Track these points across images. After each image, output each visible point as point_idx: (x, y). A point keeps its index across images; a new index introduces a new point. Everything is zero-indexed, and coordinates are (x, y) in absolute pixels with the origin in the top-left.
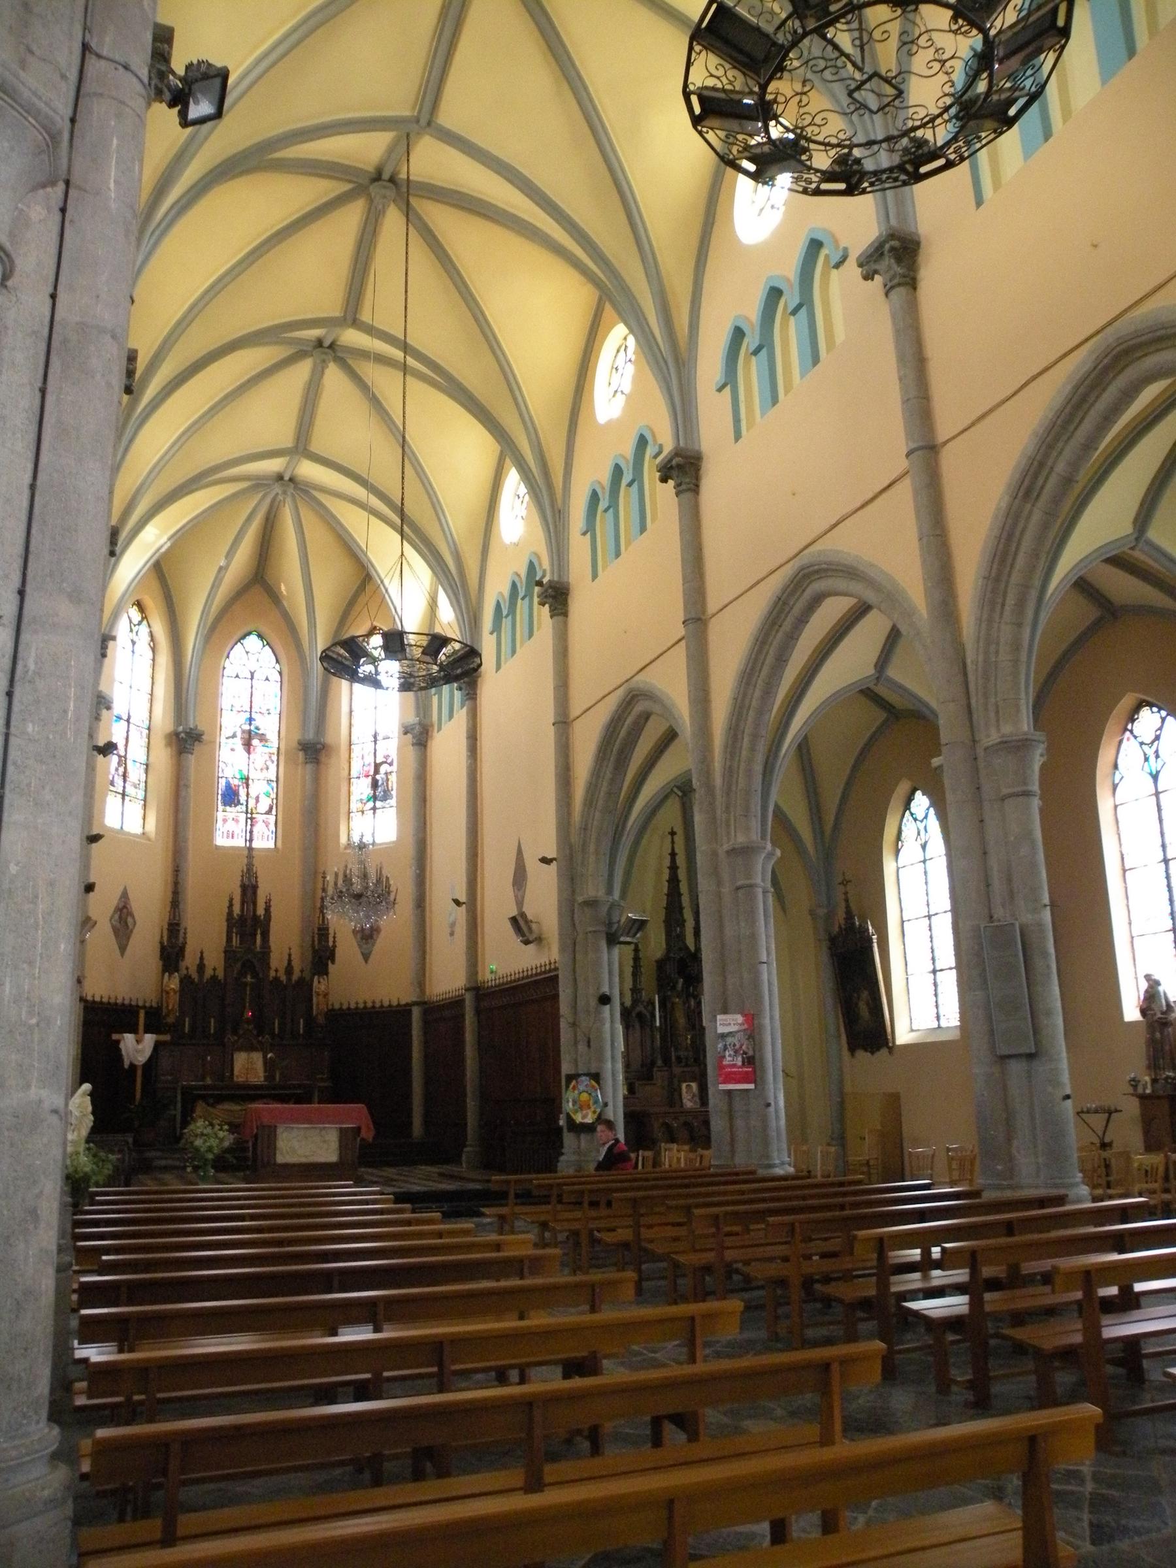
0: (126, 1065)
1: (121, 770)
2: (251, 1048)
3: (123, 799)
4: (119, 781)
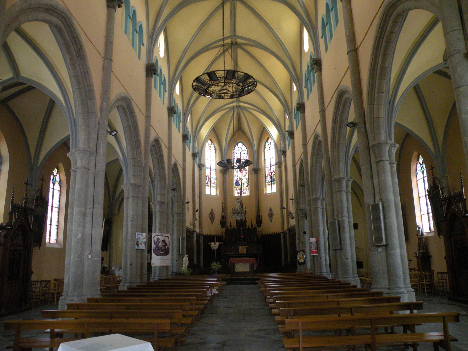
2: (243, 245)
4: (209, 183)
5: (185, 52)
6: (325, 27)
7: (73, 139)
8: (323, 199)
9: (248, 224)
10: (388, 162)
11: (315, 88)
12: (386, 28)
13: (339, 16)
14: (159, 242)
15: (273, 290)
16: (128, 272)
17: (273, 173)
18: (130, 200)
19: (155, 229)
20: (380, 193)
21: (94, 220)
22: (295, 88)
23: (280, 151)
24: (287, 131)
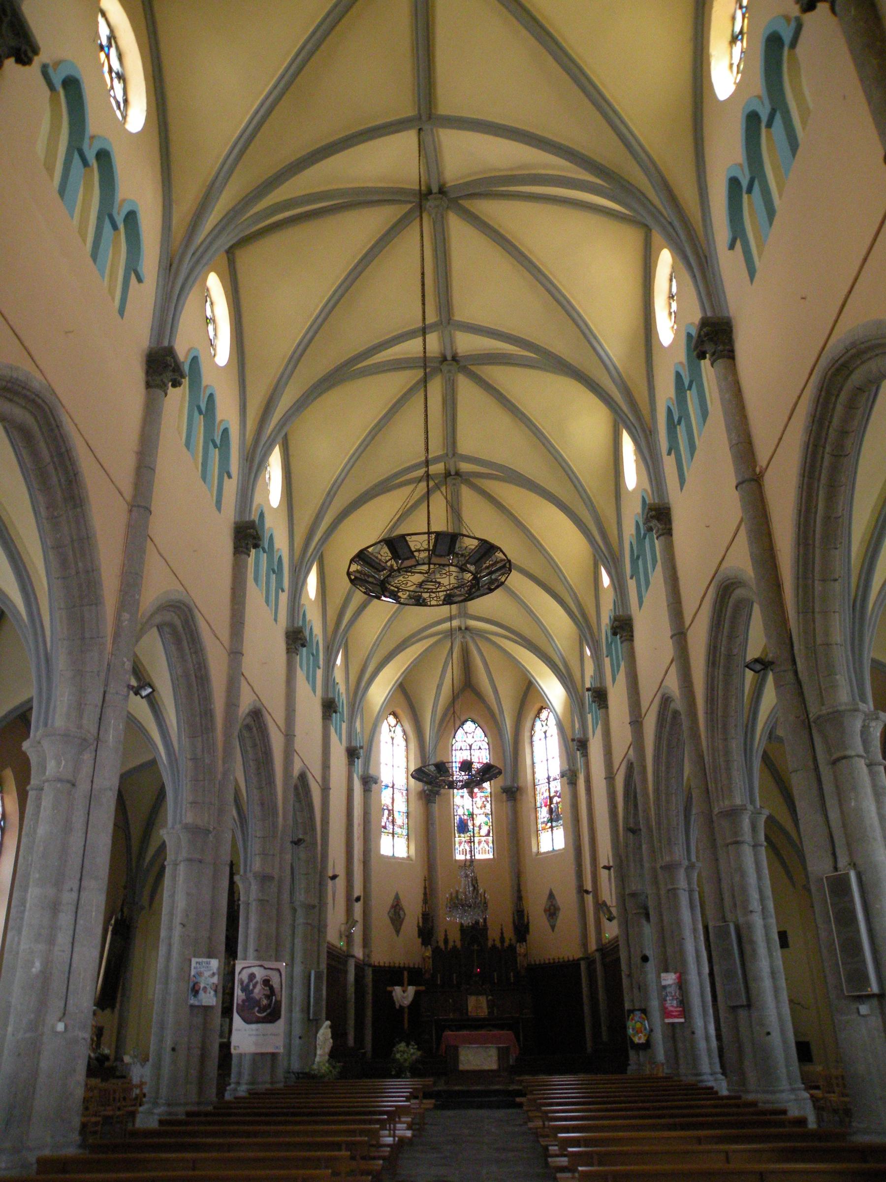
0: (397, 1007)
1: (391, 818)
2: (478, 994)
3: (393, 836)
5: (331, 495)
6: (675, 427)
7: (40, 707)
8: (691, 867)
9: (493, 934)
10: (863, 761)
11: (657, 577)
12: (830, 422)
13: (709, 402)
14: (255, 986)
15: (567, 1129)
16: (166, 1071)
17: (556, 800)
18: (182, 868)
19: (245, 949)
20: (849, 845)
21: (81, 922)
22: (606, 580)
23: (573, 740)
24: (588, 690)
